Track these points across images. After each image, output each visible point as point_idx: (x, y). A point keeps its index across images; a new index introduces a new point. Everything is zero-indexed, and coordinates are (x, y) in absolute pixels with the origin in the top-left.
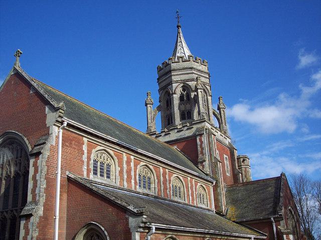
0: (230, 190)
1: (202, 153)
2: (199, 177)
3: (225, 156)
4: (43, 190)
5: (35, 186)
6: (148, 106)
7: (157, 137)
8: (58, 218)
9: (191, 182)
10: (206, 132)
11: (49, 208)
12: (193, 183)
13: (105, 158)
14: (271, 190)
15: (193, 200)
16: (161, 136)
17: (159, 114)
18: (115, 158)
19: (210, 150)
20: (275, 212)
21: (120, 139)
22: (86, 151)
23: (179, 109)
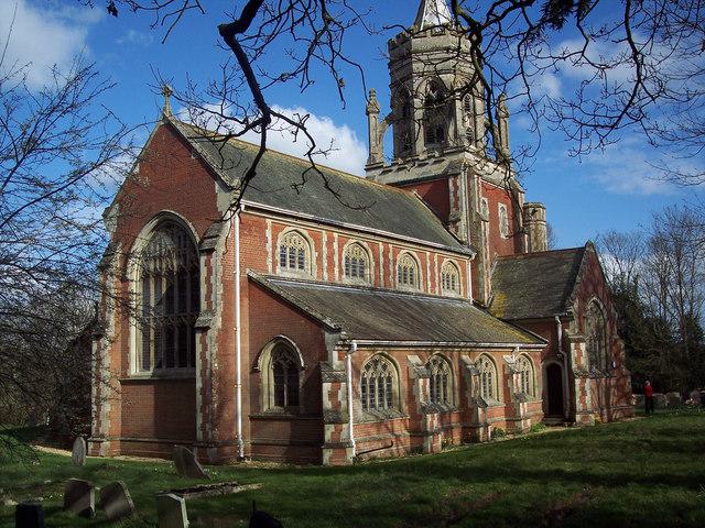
0: (504, 264)
1: (456, 205)
2: (445, 250)
3: (500, 205)
4: (219, 297)
5: (210, 291)
6: (371, 115)
8: (239, 329)
9: (432, 260)
11: (228, 318)
12: (436, 260)
14: (566, 268)
15: (433, 286)
16: (390, 171)
17: (390, 129)
18: (311, 239)
19: (470, 200)
20: (562, 307)
21: (317, 211)
22: (270, 238)
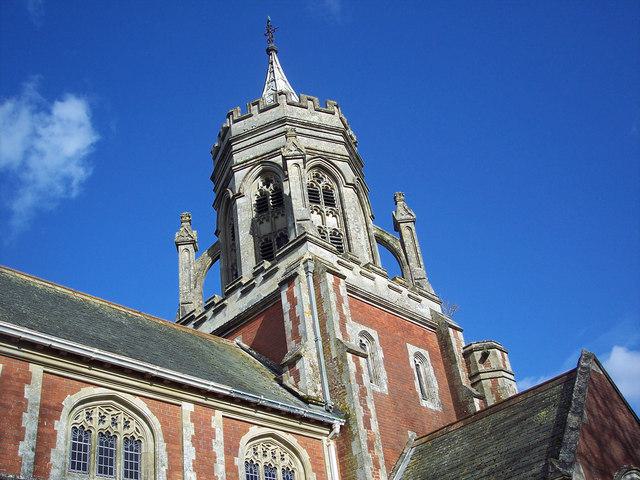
1: (297, 336)
3: (412, 349)
7: (196, 326)
9: (203, 440)
10: (306, 269)
13: (277, 454)
16: (205, 319)
18: (304, 453)
23: (253, 231)
